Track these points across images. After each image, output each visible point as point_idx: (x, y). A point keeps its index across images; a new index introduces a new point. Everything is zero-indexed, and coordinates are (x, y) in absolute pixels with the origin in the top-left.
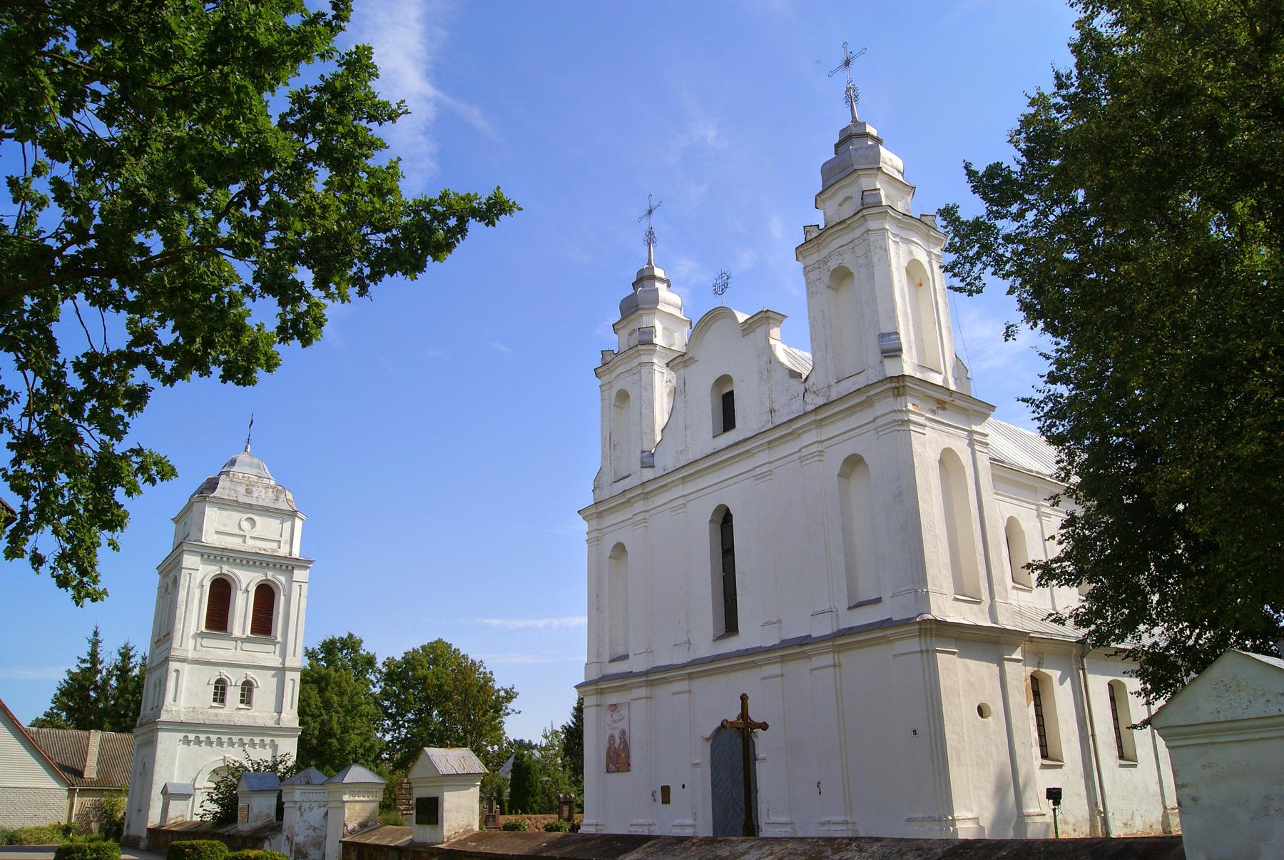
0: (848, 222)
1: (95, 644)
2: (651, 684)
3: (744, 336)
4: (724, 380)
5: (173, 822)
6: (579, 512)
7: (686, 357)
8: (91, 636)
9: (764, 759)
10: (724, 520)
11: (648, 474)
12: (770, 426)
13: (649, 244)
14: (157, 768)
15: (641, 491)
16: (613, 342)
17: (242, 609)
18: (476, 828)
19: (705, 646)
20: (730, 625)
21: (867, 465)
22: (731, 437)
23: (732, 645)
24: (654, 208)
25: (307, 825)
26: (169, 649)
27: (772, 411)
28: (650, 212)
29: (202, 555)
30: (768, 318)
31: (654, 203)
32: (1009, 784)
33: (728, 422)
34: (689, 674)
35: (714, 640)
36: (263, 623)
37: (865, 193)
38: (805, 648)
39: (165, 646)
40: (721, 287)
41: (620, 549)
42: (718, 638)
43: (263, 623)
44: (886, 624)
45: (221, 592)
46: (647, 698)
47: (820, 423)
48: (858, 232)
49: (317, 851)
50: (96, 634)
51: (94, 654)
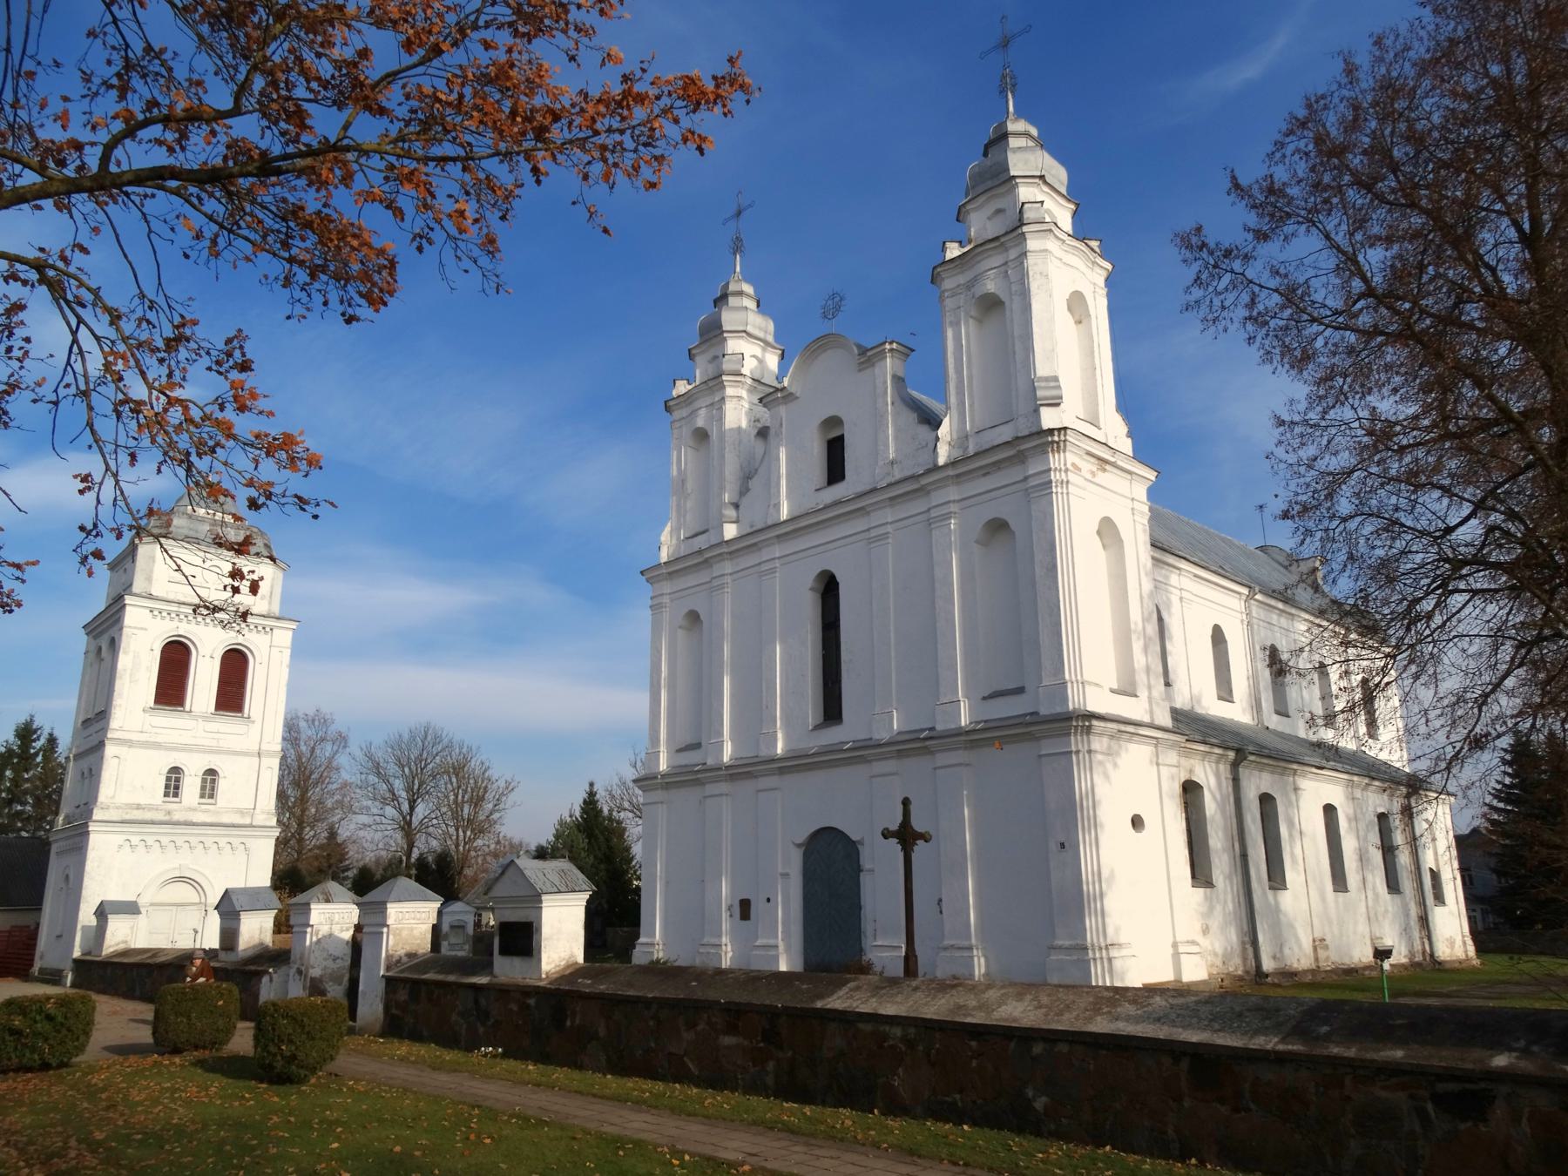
0: (1002, 240)
3: (860, 370)
4: (833, 422)
5: (112, 950)
6: (642, 573)
9: (872, 871)
10: (829, 588)
14: (87, 882)
17: (204, 679)
18: (580, 959)
20: (832, 710)
21: (1013, 533)
22: (838, 491)
23: (842, 734)
24: (745, 209)
25: (325, 955)
26: (105, 729)
33: (835, 470)
34: (780, 768)
36: (231, 695)
39: (98, 726)
43: (231, 695)
45: (175, 659)
49: (336, 987)
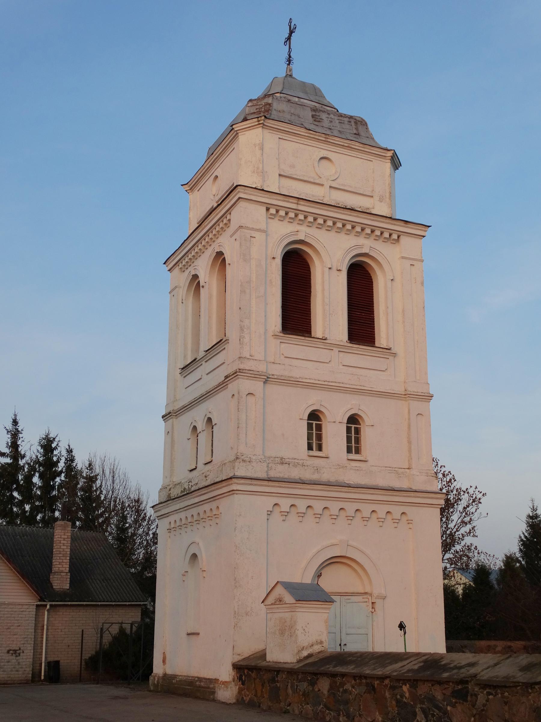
1: (15, 435)
8: (10, 426)
29: (268, 209)
30: (237, 133)
32: (151, 685)
50: (15, 422)
51: (14, 445)
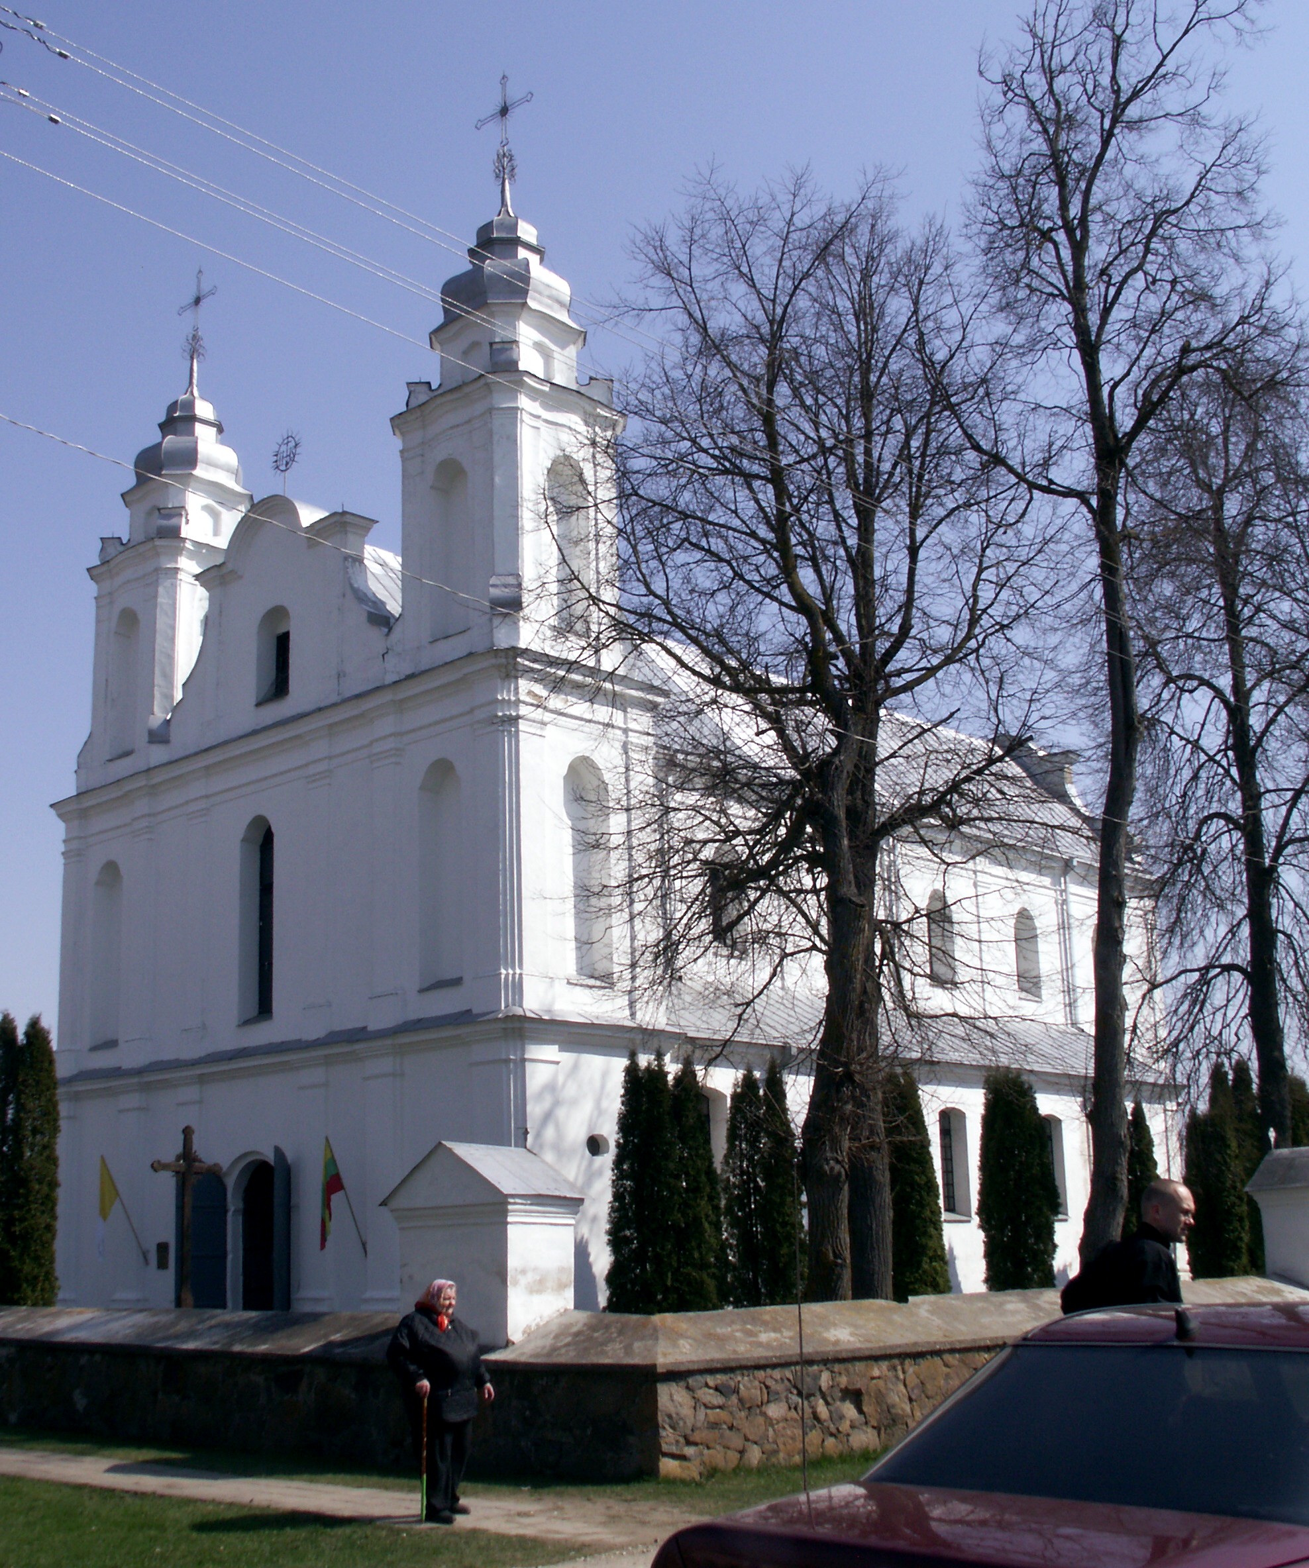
2: (146, 1088)
4: (277, 613)
7: (224, 570)
11: (158, 754)
12: (334, 698)
13: (192, 358)
15: (143, 783)
16: (120, 523)
19: (228, 1037)
23: (263, 1034)
27: (340, 675)
28: (197, 301)
31: (206, 287)
33: (279, 686)
35: (239, 1026)
37: (495, 347)
38: (357, 1047)
40: (285, 460)
41: (111, 870)
42: (247, 1023)
44: (116, 1073)
46: (139, 1109)
47: (400, 706)
48: (479, 408)
